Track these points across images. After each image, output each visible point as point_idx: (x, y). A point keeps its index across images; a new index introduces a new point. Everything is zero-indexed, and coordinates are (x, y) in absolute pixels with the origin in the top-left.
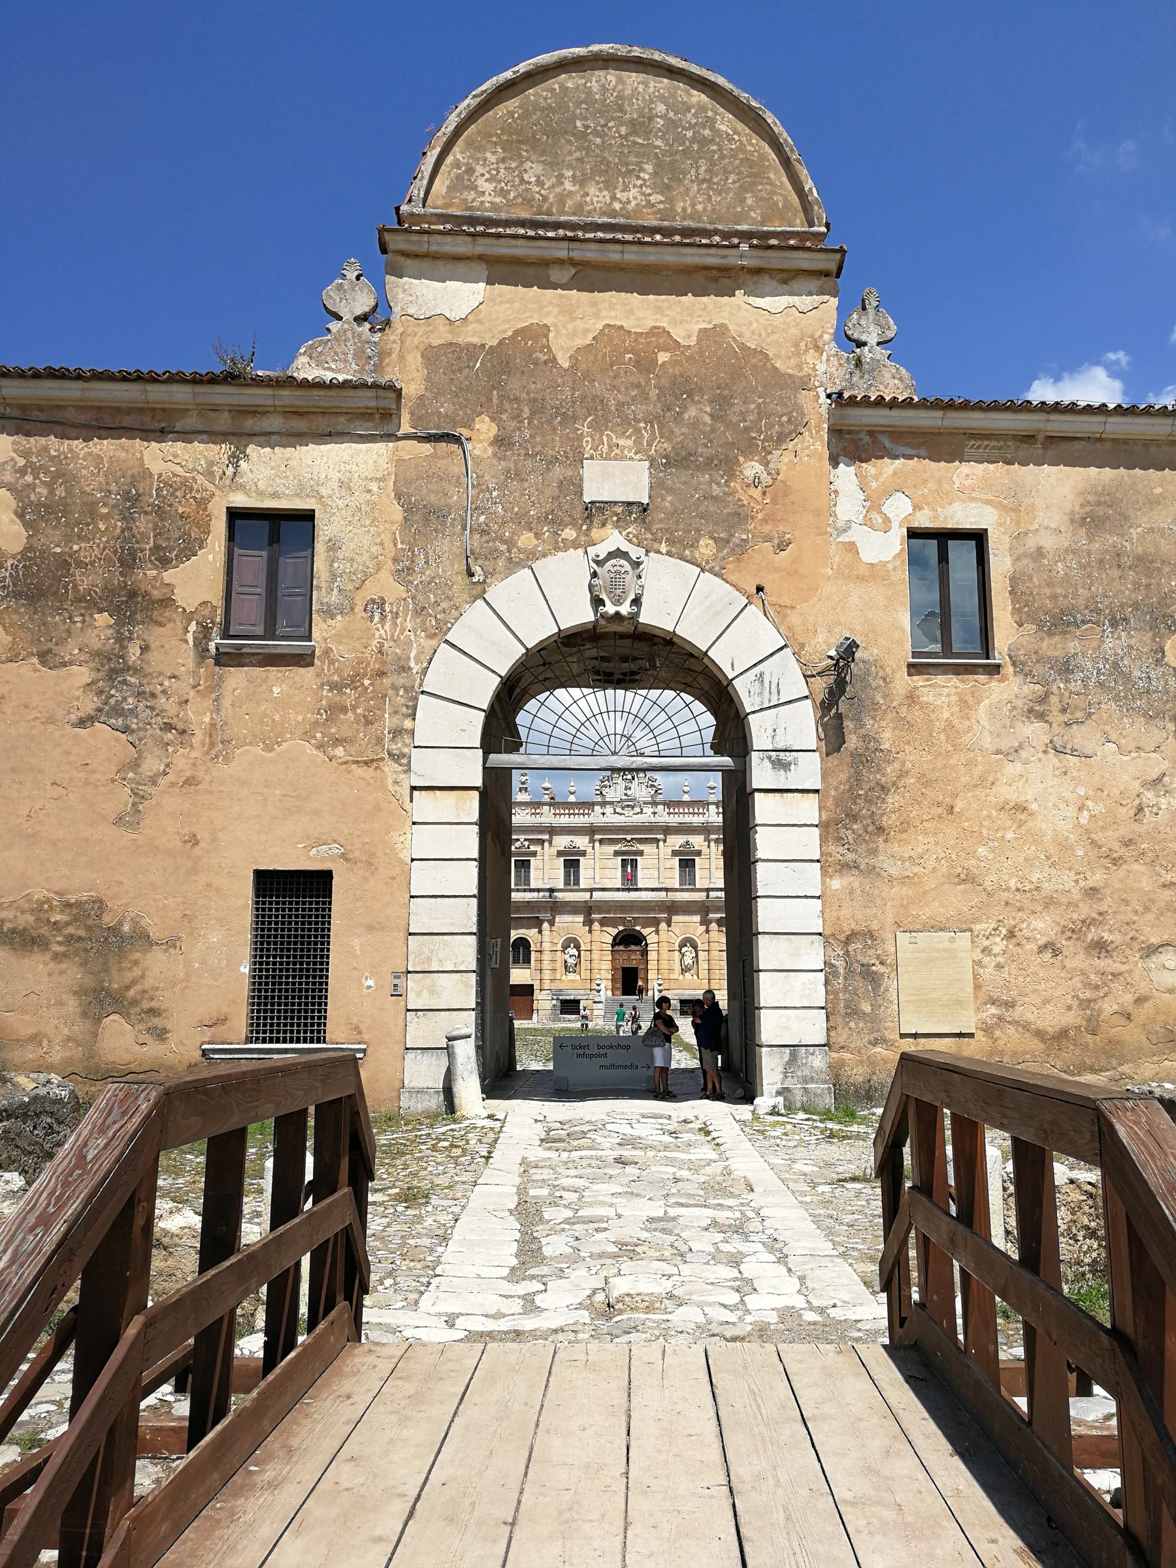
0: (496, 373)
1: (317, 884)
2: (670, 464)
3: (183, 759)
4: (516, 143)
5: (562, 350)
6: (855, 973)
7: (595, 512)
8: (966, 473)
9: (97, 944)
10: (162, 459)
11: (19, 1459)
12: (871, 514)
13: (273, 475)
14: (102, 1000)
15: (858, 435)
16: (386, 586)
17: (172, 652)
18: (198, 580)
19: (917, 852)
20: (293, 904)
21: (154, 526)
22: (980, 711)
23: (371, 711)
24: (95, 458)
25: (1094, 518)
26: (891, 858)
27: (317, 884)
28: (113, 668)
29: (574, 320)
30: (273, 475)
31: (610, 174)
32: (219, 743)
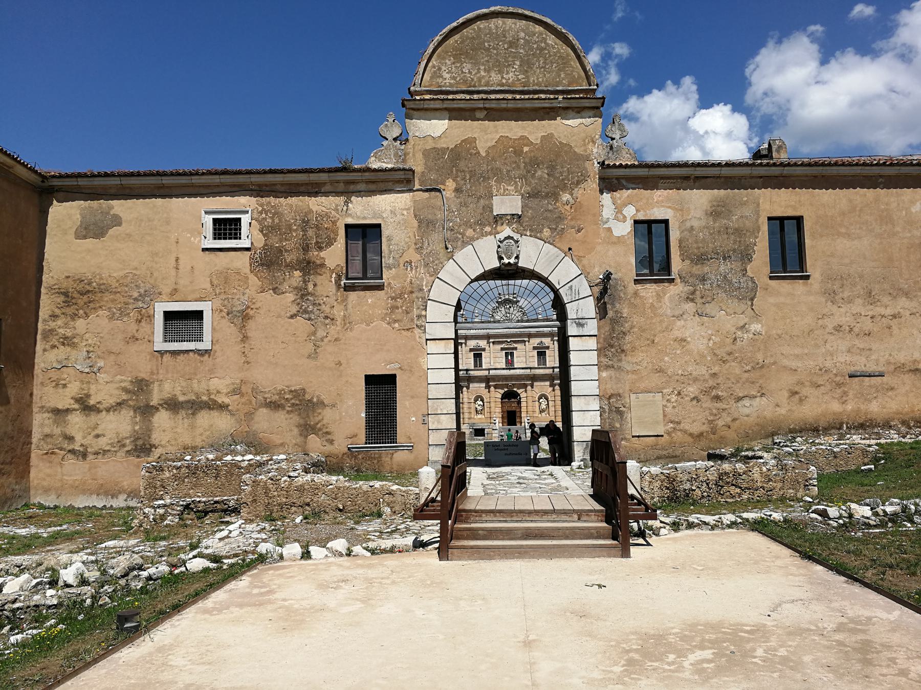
0: (454, 159)
1: (391, 379)
2: (531, 196)
3: (334, 330)
4: (459, 55)
5: (482, 148)
7: (498, 219)
8: (659, 194)
9: (303, 407)
10: (318, 204)
12: (618, 215)
13: (363, 209)
14: (307, 429)
15: (612, 180)
18: (334, 255)
19: (639, 360)
20: (381, 387)
21: (315, 234)
22: (664, 298)
23: (412, 302)
25: (716, 212)
26: (627, 363)
27: (391, 379)
28: (303, 294)
29: (487, 134)
31: (501, 68)
32: (347, 323)
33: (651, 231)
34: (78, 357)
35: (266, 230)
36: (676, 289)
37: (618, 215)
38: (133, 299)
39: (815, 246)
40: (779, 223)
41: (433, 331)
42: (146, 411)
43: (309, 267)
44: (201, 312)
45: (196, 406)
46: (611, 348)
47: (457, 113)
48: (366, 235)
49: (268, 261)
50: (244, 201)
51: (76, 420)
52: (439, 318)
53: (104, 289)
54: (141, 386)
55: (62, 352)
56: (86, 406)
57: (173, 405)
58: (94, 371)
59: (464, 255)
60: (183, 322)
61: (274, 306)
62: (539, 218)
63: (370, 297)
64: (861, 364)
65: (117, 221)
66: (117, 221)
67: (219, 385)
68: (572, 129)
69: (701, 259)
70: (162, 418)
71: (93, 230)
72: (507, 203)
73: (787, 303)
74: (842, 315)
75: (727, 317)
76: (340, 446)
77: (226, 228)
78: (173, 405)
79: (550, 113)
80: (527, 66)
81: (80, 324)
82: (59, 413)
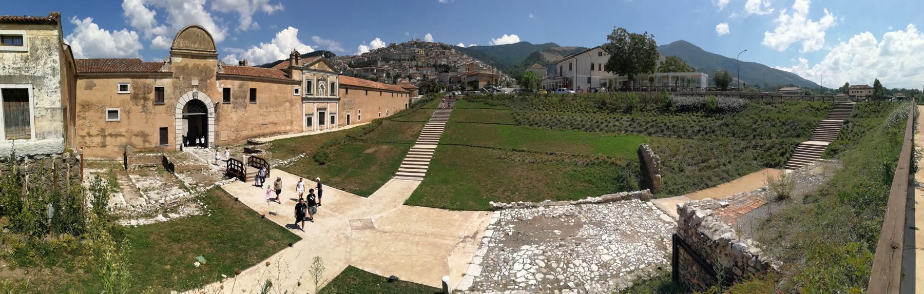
0: (183, 69)
1: (166, 129)
2: (201, 80)
3: (152, 116)
4: (185, 38)
5: (190, 66)
6: (217, 135)
7: (193, 86)
8: (229, 81)
9: (144, 136)
10: (149, 81)
11: (89, 19)
12: (220, 86)
13: (160, 83)
14: (145, 141)
15: (219, 77)
16: (172, 96)
17: (150, 104)
18: (152, 95)
19: (223, 123)
20: (164, 132)
21: (147, 90)
22: (227, 108)
23: (172, 108)
24: (141, 81)
25: (240, 87)
26: (220, 123)
27: (166, 129)
28: (144, 106)
29: (192, 62)
30: (160, 83)
31: (194, 43)
32: (155, 114)
33: (227, 92)
34: (87, 122)
35: (134, 88)
36: (231, 106)
37: (220, 86)
38: (100, 107)
39: (258, 95)
40: (251, 90)
41: (177, 116)
42: (105, 136)
43: (146, 99)
44: (117, 112)
45: (117, 135)
46: (217, 120)
47: (184, 56)
48: (160, 91)
49: (135, 97)
50: (128, 80)
51: (87, 138)
52: (179, 113)
53: (92, 104)
54: (103, 130)
55: (82, 121)
56: (90, 135)
57: (111, 135)
58: (91, 126)
59: (185, 96)
60: (113, 113)
61: (137, 109)
62: (202, 87)
63: (161, 107)
64: (264, 122)
65: (95, 85)
66: (95, 85)
67: (122, 130)
68: (211, 62)
69: (236, 98)
70: (108, 138)
71: (89, 87)
72: (195, 82)
73: (252, 107)
74: (261, 112)
75: (241, 112)
76: (153, 145)
77: (124, 87)
78: (111, 135)
79: (205, 57)
80: (201, 43)
81: (87, 114)
82: (83, 137)
